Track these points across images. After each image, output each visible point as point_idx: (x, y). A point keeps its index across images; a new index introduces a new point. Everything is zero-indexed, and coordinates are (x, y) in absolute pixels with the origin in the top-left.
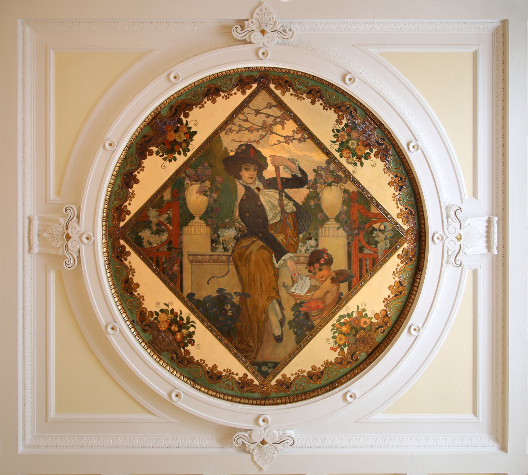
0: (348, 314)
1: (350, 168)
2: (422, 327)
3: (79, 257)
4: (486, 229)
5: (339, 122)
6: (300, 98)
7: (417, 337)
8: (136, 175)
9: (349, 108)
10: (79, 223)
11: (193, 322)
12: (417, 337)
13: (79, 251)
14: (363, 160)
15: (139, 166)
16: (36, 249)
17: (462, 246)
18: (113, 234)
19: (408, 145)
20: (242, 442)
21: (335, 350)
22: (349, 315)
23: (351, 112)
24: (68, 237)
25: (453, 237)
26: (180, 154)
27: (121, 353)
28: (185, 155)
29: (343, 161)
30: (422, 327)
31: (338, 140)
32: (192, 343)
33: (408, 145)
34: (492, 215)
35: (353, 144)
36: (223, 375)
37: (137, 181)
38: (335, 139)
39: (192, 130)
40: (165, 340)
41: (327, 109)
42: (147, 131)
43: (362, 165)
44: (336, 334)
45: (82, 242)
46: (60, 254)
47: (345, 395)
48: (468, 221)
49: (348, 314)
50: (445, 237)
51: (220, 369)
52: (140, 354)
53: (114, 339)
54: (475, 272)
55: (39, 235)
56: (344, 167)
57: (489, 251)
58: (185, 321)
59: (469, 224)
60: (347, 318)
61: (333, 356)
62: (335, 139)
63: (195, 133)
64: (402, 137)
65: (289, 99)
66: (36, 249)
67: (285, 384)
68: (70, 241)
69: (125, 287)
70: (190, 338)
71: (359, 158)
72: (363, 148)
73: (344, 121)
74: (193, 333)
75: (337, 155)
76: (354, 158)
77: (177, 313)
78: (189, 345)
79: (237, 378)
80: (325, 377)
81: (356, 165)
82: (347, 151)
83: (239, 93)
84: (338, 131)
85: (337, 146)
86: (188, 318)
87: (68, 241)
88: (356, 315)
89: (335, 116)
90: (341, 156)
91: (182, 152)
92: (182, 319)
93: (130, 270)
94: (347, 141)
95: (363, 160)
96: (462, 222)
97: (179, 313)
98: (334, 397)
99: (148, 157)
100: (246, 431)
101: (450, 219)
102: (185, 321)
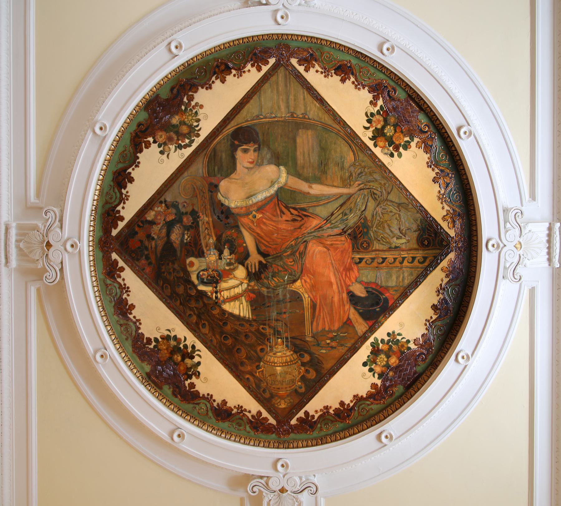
0: (181, 149)
1: (385, 159)
2: (472, 355)
3: (62, 270)
4: (547, 238)
5: (373, 103)
6: (240, 407)
7: (466, 366)
8: (130, 173)
9: (386, 87)
10: (61, 228)
11: (199, 350)
12: (466, 366)
13: (62, 263)
14: (401, 150)
15: (134, 162)
16: (14, 263)
17: (522, 257)
18: (104, 243)
19: (459, 130)
20: (259, 490)
21: (197, 104)
22: (180, 147)
23: (389, 91)
24: (49, 245)
25: (510, 246)
26: (382, 341)
27: (116, 391)
28: (376, 339)
29: (377, 151)
30: (472, 355)
31: (372, 126)
32: (198, 375)
33: (459, 130)
34: (553, 221)
35: (389, 131)
36: (233, 412)
37: (131, 180)
38: (368, 125)
39: (368, 367)
40: (167, 372)
41: (208, 394)
42: (144, 116)
43: (400, 155)
44: (195, 124)
45: (66, 249)
46: (39, 267)
47: (379, 437)
48: (530, 226)
49: (181, 149)
50: (501, 245)
51: (231, 404)
52: (127, 378)
53: (105, 372)
54: (532, 291)
55: (18, 247)
56: (380, 161)
57: (550, 265)
58: (190, 350)
59: (530, 231)
60: (183, 144)
61: (364, 390)
62: (368, 125)
63: (365, 364)
64: (451, 120)
65: (314, 77)
66: (14, 263)
67: (308, 424)
68: (52, 250)
69: (119, 309)
70: (193, 371)
71: (397, 148)
72: (402, 136)
73: (380, 102)
74: (199, 363)
75: (370, 144)
76: (391, 148)
77: (180, 339)
78: (194, 377)
79: (317, 67)
80: (355, 414)
81: (392, 155)
82: (383, 139)
83: (254, 70)
84: (372, 115)
85: (370, 134)
86: (193, 347)
87: (48, 250)
88: (171, 146)
89: (370, 97)
90: (375, 145)
91: (379, 342)
92: (186, 346)
93: (125, 289)
94: (383, 127)
95: (401, 150)
96: (522, 228)
97: (183, 339)
98: (365, 440)
99: (145, 150)
100: (261, 477)
101: (508, 223)
102: (190, 350)
